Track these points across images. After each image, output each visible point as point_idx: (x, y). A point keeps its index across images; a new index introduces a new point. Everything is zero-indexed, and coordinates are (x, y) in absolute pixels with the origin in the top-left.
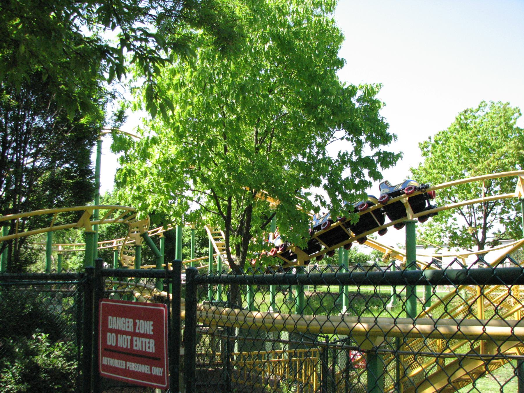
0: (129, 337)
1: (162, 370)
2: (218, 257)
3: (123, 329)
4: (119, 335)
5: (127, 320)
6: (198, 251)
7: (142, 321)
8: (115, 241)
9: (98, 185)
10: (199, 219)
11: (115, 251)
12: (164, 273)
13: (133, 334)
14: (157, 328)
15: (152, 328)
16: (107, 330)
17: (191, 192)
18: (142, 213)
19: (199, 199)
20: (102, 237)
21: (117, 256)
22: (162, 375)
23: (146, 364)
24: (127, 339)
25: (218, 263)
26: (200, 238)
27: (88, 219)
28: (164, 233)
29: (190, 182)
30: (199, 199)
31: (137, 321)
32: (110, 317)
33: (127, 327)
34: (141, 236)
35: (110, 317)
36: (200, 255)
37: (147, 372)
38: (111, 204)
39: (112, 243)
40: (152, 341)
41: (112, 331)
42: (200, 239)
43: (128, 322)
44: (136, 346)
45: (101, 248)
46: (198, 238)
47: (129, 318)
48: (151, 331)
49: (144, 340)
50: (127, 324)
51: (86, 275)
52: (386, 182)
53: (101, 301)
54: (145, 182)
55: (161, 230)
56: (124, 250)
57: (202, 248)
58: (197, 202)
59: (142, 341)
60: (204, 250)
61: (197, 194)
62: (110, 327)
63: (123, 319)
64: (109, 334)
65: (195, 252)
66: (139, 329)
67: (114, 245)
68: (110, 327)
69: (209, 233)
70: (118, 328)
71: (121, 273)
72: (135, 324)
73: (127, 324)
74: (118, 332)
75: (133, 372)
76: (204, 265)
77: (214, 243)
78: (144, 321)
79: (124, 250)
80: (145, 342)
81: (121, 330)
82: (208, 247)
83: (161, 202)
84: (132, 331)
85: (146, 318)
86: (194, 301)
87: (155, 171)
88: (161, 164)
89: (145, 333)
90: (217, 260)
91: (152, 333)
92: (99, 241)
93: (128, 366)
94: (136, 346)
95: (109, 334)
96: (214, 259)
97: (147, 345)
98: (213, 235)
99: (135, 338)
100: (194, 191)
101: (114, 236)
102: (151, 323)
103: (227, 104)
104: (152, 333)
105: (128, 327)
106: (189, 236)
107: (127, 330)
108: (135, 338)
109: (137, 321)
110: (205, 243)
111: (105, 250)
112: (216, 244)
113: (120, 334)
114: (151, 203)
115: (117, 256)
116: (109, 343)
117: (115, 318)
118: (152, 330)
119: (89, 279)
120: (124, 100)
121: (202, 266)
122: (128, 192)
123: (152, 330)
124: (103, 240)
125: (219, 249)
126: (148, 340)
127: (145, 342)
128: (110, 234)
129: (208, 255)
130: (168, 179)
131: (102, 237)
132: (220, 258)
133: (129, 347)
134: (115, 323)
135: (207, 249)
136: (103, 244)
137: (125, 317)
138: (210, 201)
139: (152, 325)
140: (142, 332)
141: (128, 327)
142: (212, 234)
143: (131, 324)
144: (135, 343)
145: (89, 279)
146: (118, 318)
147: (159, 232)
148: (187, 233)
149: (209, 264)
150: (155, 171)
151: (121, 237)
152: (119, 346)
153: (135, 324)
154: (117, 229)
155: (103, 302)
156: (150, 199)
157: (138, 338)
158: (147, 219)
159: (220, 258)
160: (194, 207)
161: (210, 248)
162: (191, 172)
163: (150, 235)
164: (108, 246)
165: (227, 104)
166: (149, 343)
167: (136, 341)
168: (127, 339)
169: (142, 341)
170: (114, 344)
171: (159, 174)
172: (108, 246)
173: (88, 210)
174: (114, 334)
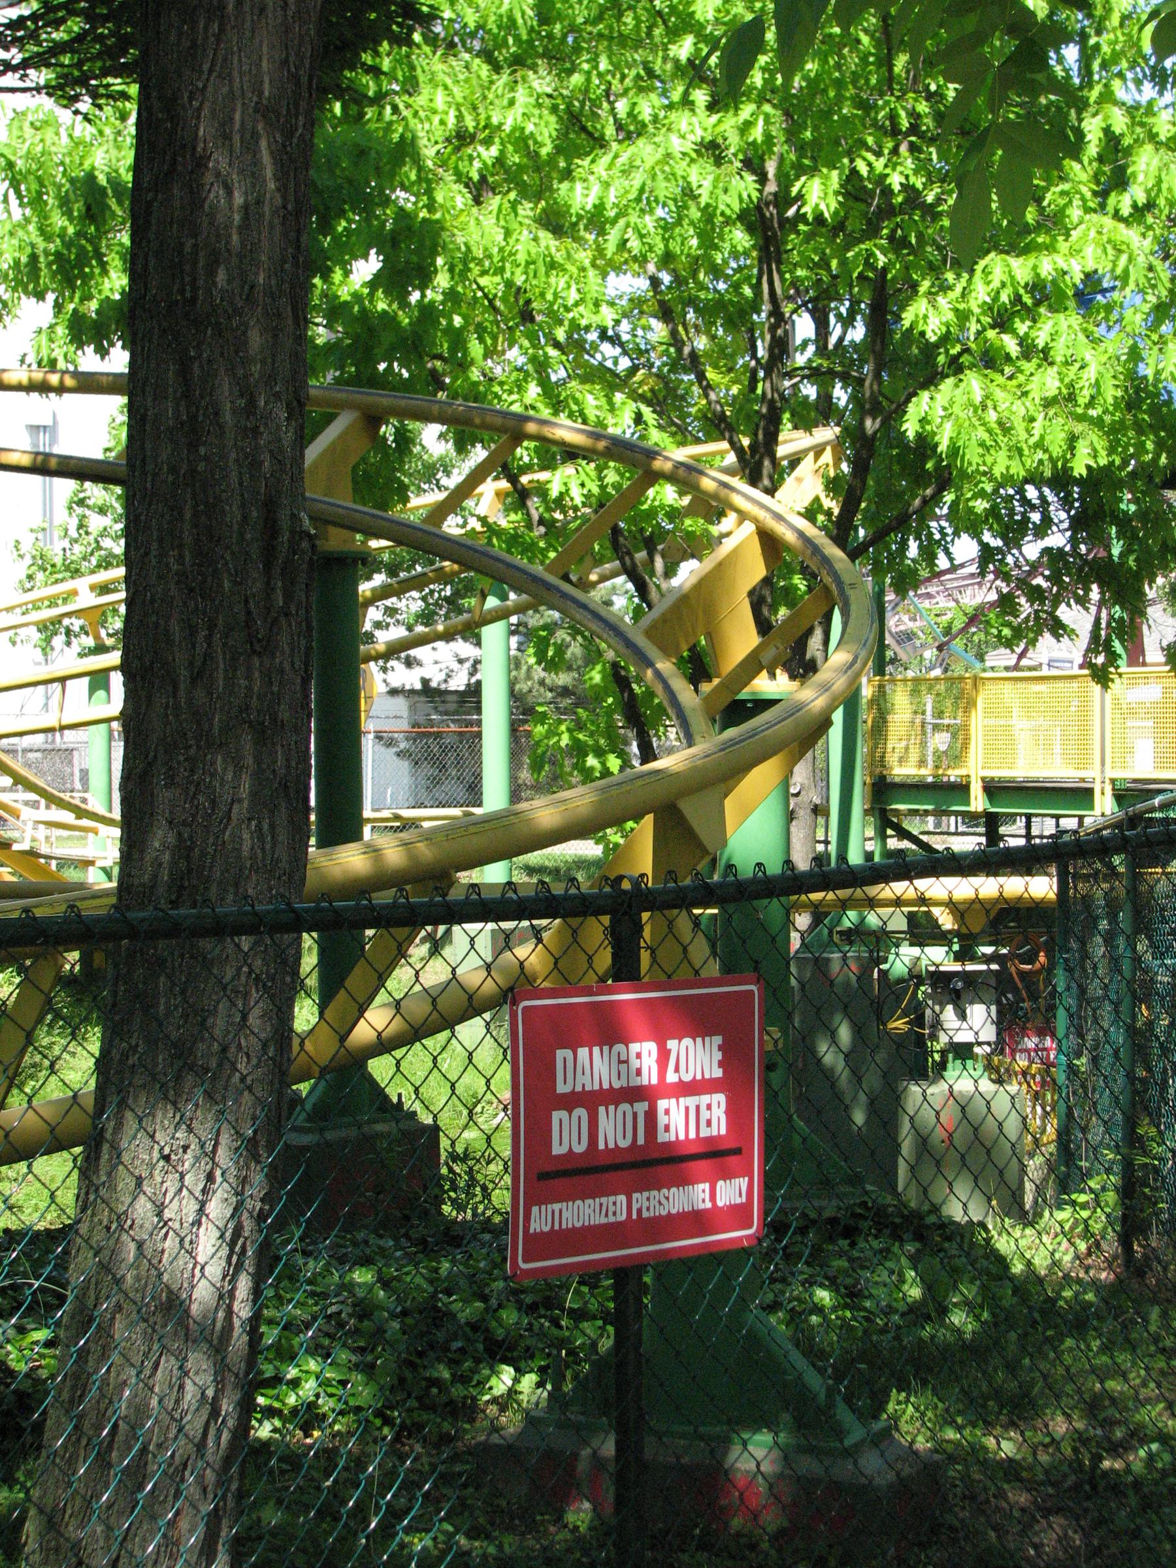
3: (617, 1085)
4: (602, 1109)
24: (635, 1115)
31: (672, 1044)
102: (718, 1040)
133: (641, 1141)
139: (720, 1048)
167: (667, 1112)
168: (635, 1115)
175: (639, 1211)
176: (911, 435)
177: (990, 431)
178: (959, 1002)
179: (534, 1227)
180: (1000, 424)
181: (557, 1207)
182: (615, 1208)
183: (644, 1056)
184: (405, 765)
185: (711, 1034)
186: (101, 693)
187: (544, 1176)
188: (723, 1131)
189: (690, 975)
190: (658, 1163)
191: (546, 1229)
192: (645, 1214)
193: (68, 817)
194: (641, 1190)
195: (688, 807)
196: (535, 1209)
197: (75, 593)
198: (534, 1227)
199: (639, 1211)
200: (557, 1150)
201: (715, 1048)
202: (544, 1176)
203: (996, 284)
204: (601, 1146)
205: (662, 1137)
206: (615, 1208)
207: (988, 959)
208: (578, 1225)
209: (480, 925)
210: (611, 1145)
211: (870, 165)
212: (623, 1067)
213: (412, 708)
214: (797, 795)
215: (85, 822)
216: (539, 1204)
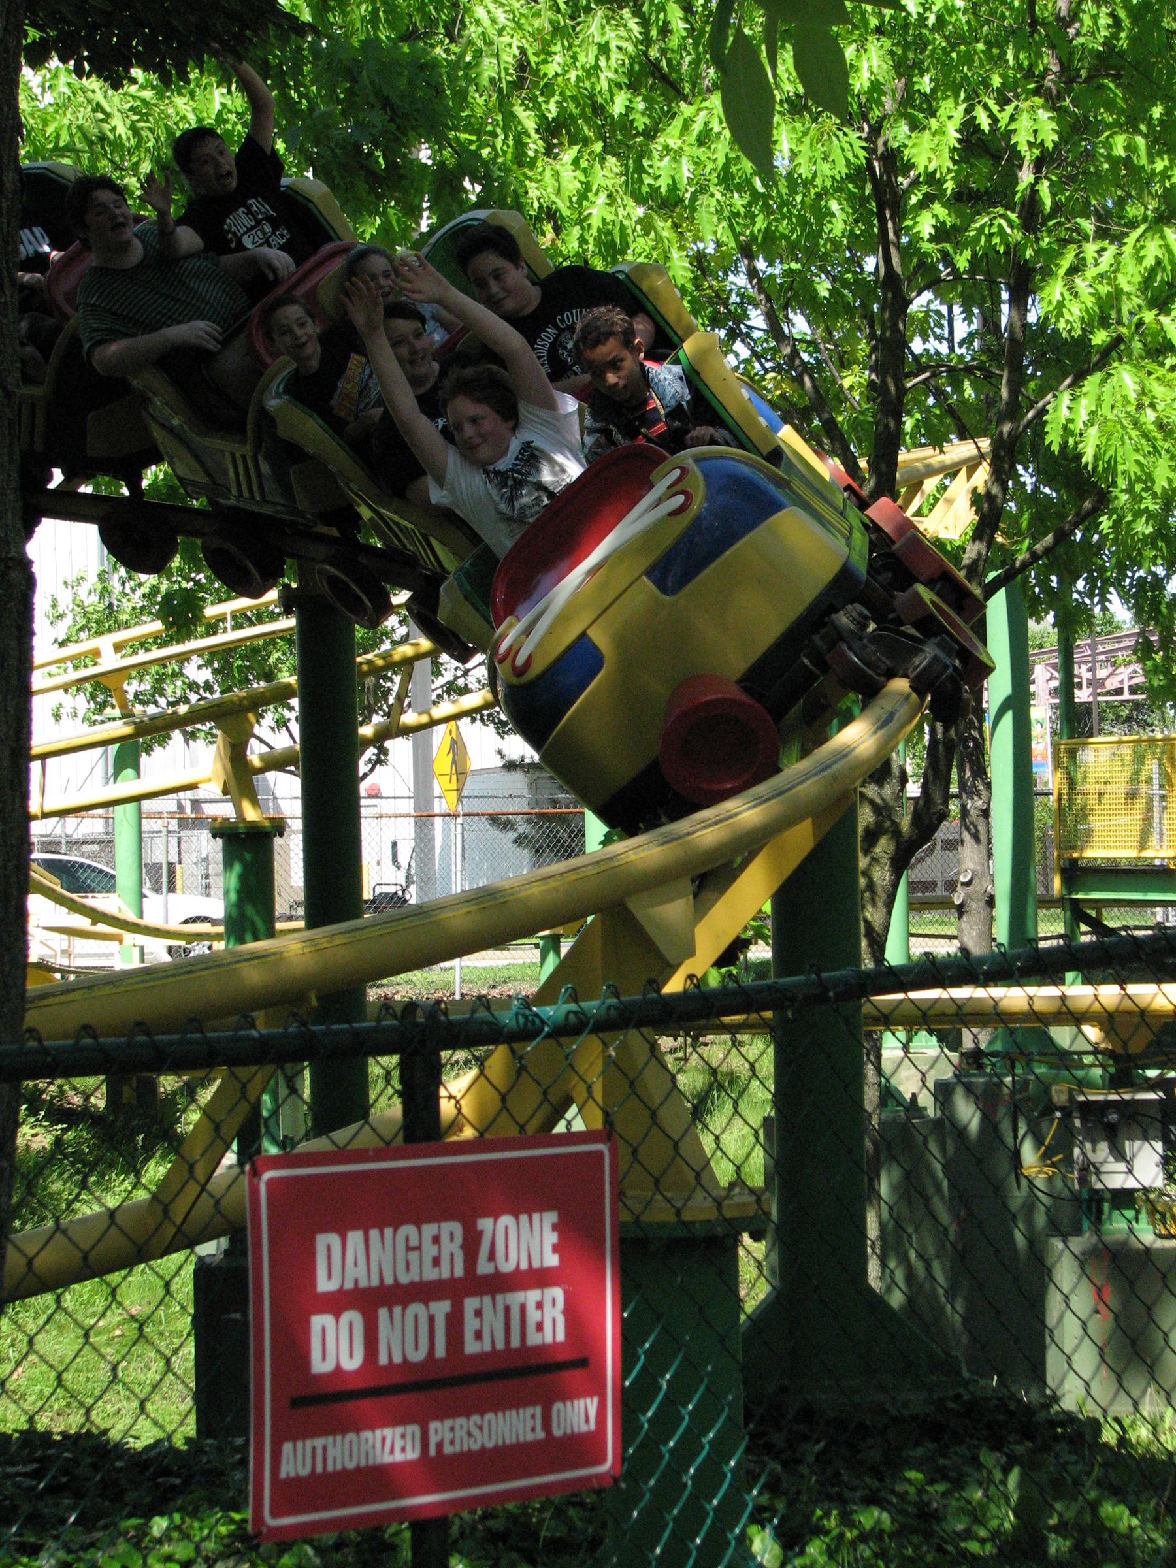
1: (293, 268)
3: (404, 1279)
4: (383, 1313)
5: (429, 1229)
7: (506, 1220)
15: (551, 1238)
22: (592, 1426)
23: (518, 1403)
24: (432, 1319)
31: (485, 1224)
37: (530, 1437)
43: (436, 1240)
44: (478, 1335)
48: (548, 1248)
50: (430, 1250)
52: (113, 877)
63: (408, 1230)
66: (492, 1257)
75: (466, 1457)
89: (524, 1266)
91: (552, 1260)
93: (433, 1440)
94: (478, 1335)
102: (551, 1217)
103: (898, 245)
116: (320, 1365)
118: (556, 1249)
120: (453, 1102)
133: (441, 1351)
139: (555, 1227)
144: (470, 1324)
146: (374, 1233)
165: (898, 245)
167: (478, 1313)
168: (432, 1319)
174: (351, 1317)
175: (440, 1446)
176: (1055, 448)
177: (1145, 435)
178: (1114, 1138)
179: (286, 1470)
180: (1161, 426)
181: (319, 1442)
182: (516, 1426)
183: (445, 1238)
184: (525, 854)
185: (542, 1209)
186: (129, 772)
187: (299, 1402)
188: (561, 1337)
189: (514, 1132)
190: (533, 1374)
191: (304, 1472)
192: (448, 1449)
193: (83, 922)
194: (441, 1417)
195: (634, 905)
196: (287, 1447)
197: (96, 653)
198: (286, 1470)
199: (440, 1446)
200: (320, 1365)
201: (547, 1228)
202: (299, 1402)
203: (1150, 261)
204: (383, 1360)
205: (534, 1339)
206: (516, 1426)
207: (1152, 1085)
208: (351, 1465)
209: (253, 1069)
210: (397, 1359)
211: (991, 115)
212: (414, 1256)
213: (533, 786)
214: (968, 884)
215: (101, 928)
216: (294, 1439)
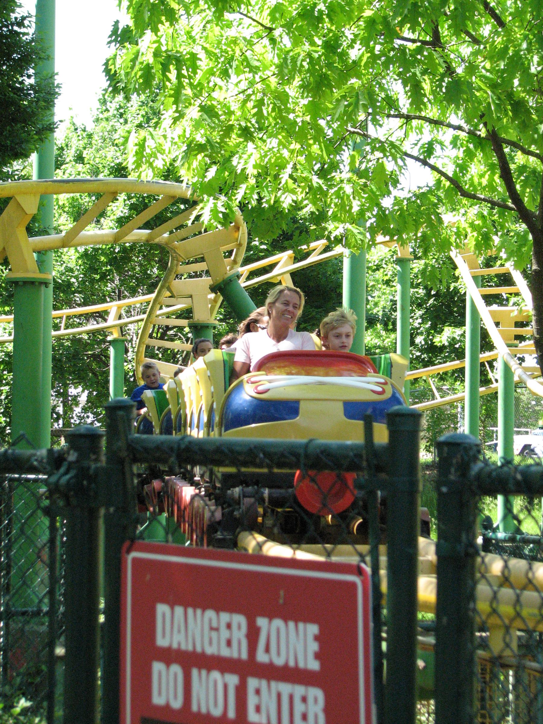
0: (233, 680)
2: (499, 365)
4: (195, 672)
5: (225, 617)
6: (419, 340)
7: (278, 623)
8: (112, 307)
9: (47, 94)
10: (430, 225)
11: (113, 342)
12: (358, 456)
13: (246, 669)
14: (334, 648)
15: (314, 646)
16: (150, 652)
17: (397, 122)
18: (219, 204)
19: (429, 149)
20: (64, 291)
21: (121, 359)
24: (226, 687)
25: (499, 386)
26: (428, 290)
27: (22, 232)
28: (294, 275)
29: (398, 90)
30: (429, 149)
31: (262, 622)
32: (162, 609)
33: (223, 643)
34: (214, 289)
35: (162, 609)
36: (433, 351)
38: (96, 172)
39: (102, 315)
40: (316, 694)
41: (169, 656)
42: (429, 295)
43: (229, 626)
45: (62, 332)
46: (421, 292)
47: (232, 610)
48: (311, 656)
49: (285, 688)
50: (225, 634)
51: (72, 457)
53: (129, 551)
54: (228, 93)
55: (284, 263)
56: (148, 341)
57: (436, 329)
58: (425, 163)
59: (279, 696)
60: (446, 335)
61: (420, 130)
62: (162, 642)
63: (210, 614)
64: (158, 667)
65: (412, 343)
66: (267, 650)
67: (112, 320)
68: (162, 642)
69: (464, 271)
70: (190, 648)
71: (201, 450)
72: (253, 634)
73: (225, 634)
74: (192, 661)
76: (443, 394)
77: (486, 313)
78: (286, 620)
79: (148, 341)
80: (291, 697)
81: (203, 655)
82: (462, 323)
83: (289, 170)
84: (244, 656)
85: (293, 613)
86: (467, 555)
87: (264, 53)
88: (288, 26)
90: (497, 375)
91: (314, 665)
92: (55, 308)
95: (158, 667)
96: (484, 373)
97: (299, 708)
98: (481, 281)
99: (252, 683)
100: (408, 118)
101: (109, 287)
102: (313, 629)
104: (314, 665)
105: (229, 643)
106: (387, 283)
107: (225, 652)
108: (252, 683)
109: (262, 622)
110: (447, 308)
111: (76, 341)
112: (493, 314)
113: (200, 668)
114: (251, 171)
115: (121, 359)
116: (158, 700)
117: (179, 610)
118: (317, 656)
119: (83, 472)
121: (439, 400)
122: (172, 136)
123: (317, 656)
124: (70, 304)
125: (504, 335)
126: (299, 690)
127: (291, 697)
128: (93, 281)
129: (460, 354)
130: (318, 86)
131: (64, 291)
132: (507, 369)
133: (232, 714)
134: (178, 626)
135: (458, 331)
136: (69, 317)
137: (218, 609)
138: (470, 155)
139: (317, 638)
140: (279, 662)
141: (229, 643)
142: (475, 278)
143: (240, 634)
144: (252, 700)
145: (83, 472)
147: (276, 271)
148: (379, 275)
149: (464, 391)
150: (264, 53)
151: (133, 292)
152: (195, 708)
153: (253, 634)
154: (120, 259)
155: (134, 554)
156: (249, 159)
157: (264, 683)
158: (237, 228)
159: (507, 369)
160: (415, 179)
161: (467, 328)
162: (405, 60)
163: (243, 283)
164: (92, 326)
166: (304, 699)
167: (258, 692)
169: (279, 696)
170: (177, 704)
171: (286, 68)
172: (92, 326)
173: (19, 198)
174: (176, 669)
